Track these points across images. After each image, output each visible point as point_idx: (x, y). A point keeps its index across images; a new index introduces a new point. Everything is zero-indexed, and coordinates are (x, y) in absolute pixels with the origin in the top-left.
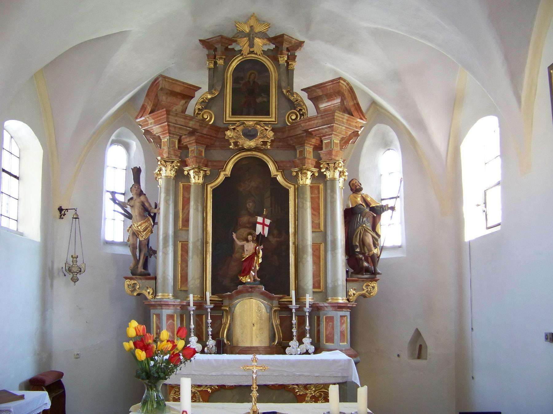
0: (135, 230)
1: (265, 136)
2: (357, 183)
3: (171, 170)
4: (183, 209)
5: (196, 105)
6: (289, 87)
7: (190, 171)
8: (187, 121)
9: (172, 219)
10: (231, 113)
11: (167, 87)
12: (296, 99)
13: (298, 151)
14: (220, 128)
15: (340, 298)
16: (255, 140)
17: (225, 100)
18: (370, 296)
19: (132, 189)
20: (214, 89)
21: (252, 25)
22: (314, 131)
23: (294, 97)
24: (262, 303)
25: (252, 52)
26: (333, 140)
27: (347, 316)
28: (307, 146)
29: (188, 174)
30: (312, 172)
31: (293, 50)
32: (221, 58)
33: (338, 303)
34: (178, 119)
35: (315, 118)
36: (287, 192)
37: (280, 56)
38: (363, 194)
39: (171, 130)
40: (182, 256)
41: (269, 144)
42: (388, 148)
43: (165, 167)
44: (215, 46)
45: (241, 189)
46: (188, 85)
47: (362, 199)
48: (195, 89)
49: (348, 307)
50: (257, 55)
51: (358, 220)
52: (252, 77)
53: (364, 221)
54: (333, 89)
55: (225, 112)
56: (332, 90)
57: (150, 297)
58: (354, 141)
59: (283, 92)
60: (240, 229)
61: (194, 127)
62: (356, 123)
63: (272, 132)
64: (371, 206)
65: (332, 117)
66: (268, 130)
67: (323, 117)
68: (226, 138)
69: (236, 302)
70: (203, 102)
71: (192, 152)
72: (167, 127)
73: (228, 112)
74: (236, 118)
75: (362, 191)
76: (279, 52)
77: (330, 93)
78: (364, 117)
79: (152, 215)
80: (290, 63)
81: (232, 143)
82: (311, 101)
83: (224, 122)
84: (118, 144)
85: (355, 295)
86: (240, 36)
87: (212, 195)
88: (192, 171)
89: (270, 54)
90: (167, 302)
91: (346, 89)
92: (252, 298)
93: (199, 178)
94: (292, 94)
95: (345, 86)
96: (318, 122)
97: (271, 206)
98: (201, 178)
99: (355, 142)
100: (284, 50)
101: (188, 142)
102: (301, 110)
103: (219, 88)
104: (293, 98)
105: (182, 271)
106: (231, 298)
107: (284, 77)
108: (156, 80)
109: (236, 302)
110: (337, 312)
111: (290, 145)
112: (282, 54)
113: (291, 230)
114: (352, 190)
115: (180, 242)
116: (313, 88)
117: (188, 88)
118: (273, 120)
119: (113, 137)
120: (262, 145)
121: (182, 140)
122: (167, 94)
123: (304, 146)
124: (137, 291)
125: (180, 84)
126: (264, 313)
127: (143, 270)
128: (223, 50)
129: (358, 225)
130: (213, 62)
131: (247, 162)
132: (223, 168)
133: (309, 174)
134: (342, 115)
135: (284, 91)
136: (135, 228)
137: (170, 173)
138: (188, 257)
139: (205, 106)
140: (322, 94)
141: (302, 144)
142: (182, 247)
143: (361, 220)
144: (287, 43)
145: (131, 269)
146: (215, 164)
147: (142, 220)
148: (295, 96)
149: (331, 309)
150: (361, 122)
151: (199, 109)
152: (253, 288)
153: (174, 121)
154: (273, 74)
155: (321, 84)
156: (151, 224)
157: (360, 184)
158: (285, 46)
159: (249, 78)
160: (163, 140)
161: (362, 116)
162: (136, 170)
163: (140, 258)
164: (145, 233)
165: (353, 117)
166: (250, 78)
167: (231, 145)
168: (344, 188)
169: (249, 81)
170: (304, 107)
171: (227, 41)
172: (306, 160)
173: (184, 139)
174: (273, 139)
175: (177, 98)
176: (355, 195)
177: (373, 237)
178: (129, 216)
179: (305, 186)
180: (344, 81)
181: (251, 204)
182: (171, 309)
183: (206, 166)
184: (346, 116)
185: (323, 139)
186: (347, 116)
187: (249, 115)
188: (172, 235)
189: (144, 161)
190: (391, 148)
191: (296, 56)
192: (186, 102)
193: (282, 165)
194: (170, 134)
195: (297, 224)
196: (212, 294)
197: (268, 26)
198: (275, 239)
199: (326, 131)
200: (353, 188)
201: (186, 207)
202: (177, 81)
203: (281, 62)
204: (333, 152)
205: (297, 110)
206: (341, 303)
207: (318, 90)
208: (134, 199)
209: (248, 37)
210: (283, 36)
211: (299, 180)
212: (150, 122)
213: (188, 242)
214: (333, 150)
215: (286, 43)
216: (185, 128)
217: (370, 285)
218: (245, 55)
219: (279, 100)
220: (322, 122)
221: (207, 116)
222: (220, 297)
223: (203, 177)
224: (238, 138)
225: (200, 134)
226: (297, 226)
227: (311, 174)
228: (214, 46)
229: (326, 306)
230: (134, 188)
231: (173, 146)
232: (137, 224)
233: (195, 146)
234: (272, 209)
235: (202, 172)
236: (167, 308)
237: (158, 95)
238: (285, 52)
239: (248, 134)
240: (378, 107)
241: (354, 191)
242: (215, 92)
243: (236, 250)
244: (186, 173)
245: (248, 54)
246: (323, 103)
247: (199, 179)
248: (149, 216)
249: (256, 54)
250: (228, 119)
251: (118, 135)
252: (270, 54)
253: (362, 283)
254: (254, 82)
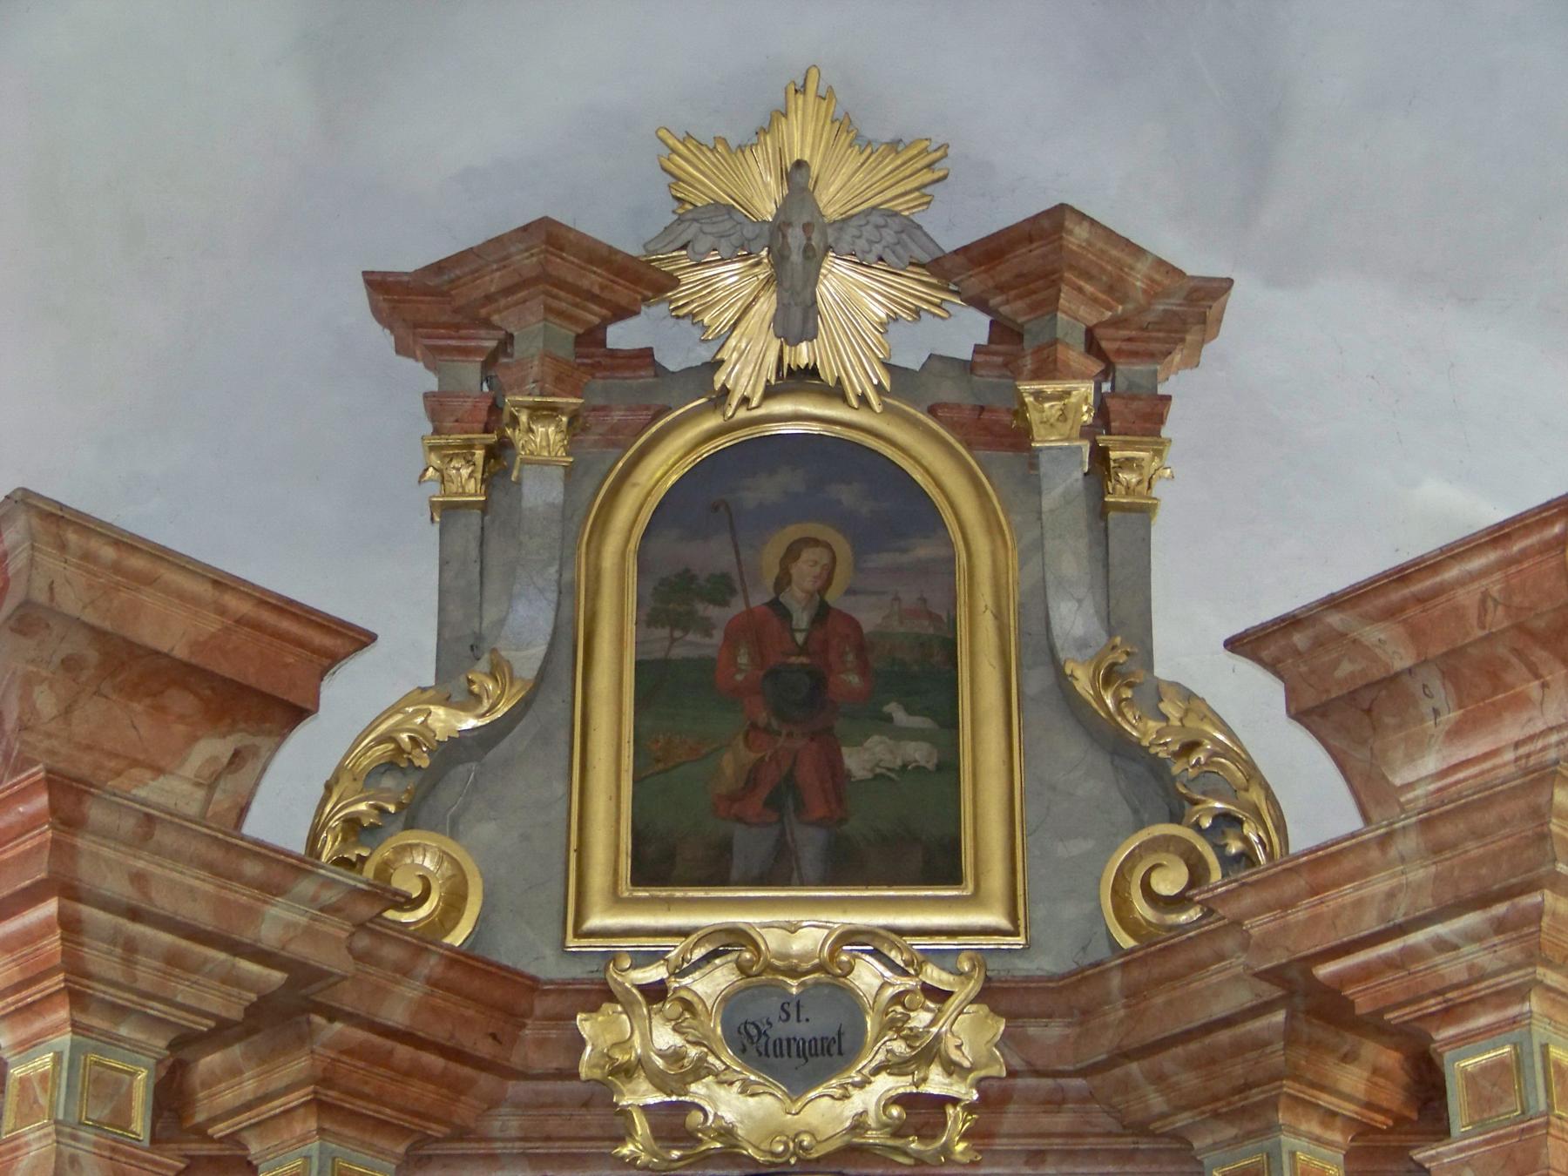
1: (929, 1047)
6: (1118, 640)
8: (241, 895)
11: (71, 601)
12: (1188, 738)
14: (533, 986)
16: (842, 1086)
20: (484, 665)
22: (1366, 973)
23: (1166, 718)
25: (800, 379)
26: (1545, 1048)
32: (543, 412)
34: (158, 871)
35: (1374, 854)
37: (1036, 386)
39: (93, 968)
41: (956, 1120)
46: (262, 603)
48: (327, 641)
50: (843, 398)
52: (806, 570)
54: (1508, 607)
55: (573, 856)
56: (1500, 611)
63: (983, 1009)
65: (1529, 829)
67: (1446, 831)
70: (389, 766)
72: (53, 943)
74: (670, 904)
76: (1028, 363)
77: (1488, 638)
80: (1113, 455)
81: (641, 1125)
82: (1308, 727)
94: (1153, 695)
96: (1400, 888)
100: (1067, 345)
101: (248, 1106)
102: (1227, 821)
104: (1153, 725)
111: (1141, 1129)
116: (1335, 619)
117: (257, 626)
120: (898, 1131)
128: (566, 351)
135: (1083, 683)
139: (404, 798)
140: (1408, 662)
144: (1088, 288)
148: (1171, 709)
151: (353, 826)
153: (116, 886)
154: (981, 545)
155: (1401, 575)
159: (783, 581)
160: (16, 1072)
166: (789, 583)
169: (777, 607)
170: (1256, 795)
171: (593, 280)
173: (209, 1083)
174: (999, 1070)
185: (1450, 1042)
187: (785, 882)
191: (1168, 398)
194: (84, 1009)
197: (929, 166)
199: (1471, 968)
202: (161, 555)
204: (1550, 1141)
205: (1197, 827)
207: (1373, 634)
210: (1059, 228)
214: (1548, 1124)
215: (1080, 290)
216: (222, 956)
220: (1437, 877)
224: (699, 1070)
225: (359, 1035)
231: (102, 1113)
233: (314, 1146)
238: (1074, 355)
239: (780, 1030)
245: (770, 393)
246: (1417, 748)
249: (836, 393)
252: (949, 391)
254: (823, 613)
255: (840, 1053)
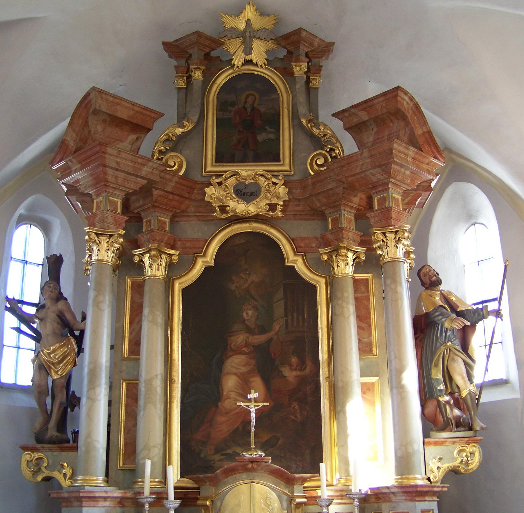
0: (44, 360)
2: (432, 272)
3: (108, 250)
4: (131, 323)
5: (156, 145)
6: (311, 114)
7: (143, 256)
9: (108, 336)
10: (214, 159)
11: (103, 109)
13: (330, 219)
15: (418, 476)
17: (205, 142)
18: (468, 470)
19: (45, 290)
20: (186, 119)
21: (249, 18)
24: (272, 489)
26: (392, 194)
27: (433, 510)
28: (345, 210)
29: (141, 260)
30: (355, 254)
31: (316, 58)
33: (416, 486)
34: (122, 161)
36: (312, 289)
38: (442, 290)
40: (127, 405)
41: (279, 208)
42: (473, 221)
43: (97, 244)
44: (188, 51)
45: (233, 287)
47: (443, 299)
48: (153, 115)
49: (434, 493)
50: (258, 66)
51: (439, 335)
53: (449, 336)
57: (66, 483)
58: (424, 201)
59: (301, 123)
60: (231, 356)
61: (149, 177)
62: (428, 164)
64: (458, 310)
66: (278, 184)
68: (207, 198)
69: (223, 489)
70: (167, 140)
71: (148, 224)
73: (209, 156)
74: (223, 166)
75: (441, 286)
76: (294, 59)
78: (441, 155)
79: (77, 333)
80: (311, 77)
83: (203, 174)
84: (32, 223)
85: (442, 470)
86: (229, 35)
87: (181, 298)
88: (148, 255)
89: (279, 65)
90: (91, 492)
91: (408, 108)
92: (255, 482)
93: (159, 267)
95: (407, 103)
97: (286, 315)
98: (162, 268)
99: (425, 203)
100: (301, 56)
102: (332, 150)
103: (195, 118)
104: (318, 131)
105: (128, 433)
106: (215, 482)
107: (302, 98)
108: (86, 96)
109: (223, 489)
110: (414, 502)
112: (298, 60)
113: (323, 355)
114: (423, 284)
115: (124, 380)
116: (353, 110)
117: (141, 113)
118: (287, 168)
119: (21, 210)
121: (132, 204)
122: (104, 121)
123: (340, 209)
124: (43, 472)
125: (127, 105)
126: (277, 510)
127: (55, 434)
128: (202, 57)
129: (438, 344)
130: (185, 78)
131: (243, 241)
132: (201, 252)
133: (351, 256)
134: (405, 147)
135: (304, 121)
136: (44, 357)
137: (105, 255)
138: (137, 408)
141: (336, 207)
142: (127, 390)
143: (444, 334)
145: (35, 431)
146: (188, 244)
147: (57, 343)
149: (404, 498)
150: (435, 163)
151: (160, 152)
152: (255, 461)
153: (114, 165)
156: (74, 350)
157: (437, 274)
158: (303, 49)
159: (246, 102)
161: (436, 154)
162: (53, 260)
163: (52, 412)
164: (61, 365)
165: (423, 154)
167: (215, 211)
168: (410, 280)
169: (244, 107)
171: (207, 43)
172: (344, 232)
175: (122, 129)
176: (429, 292)
177: (466, 363)
178: (37, 338)
179: (344, 278)
180: (406, 93)
181: (250, 312)
182: (99, 506)
183: (173, 248)
184: (412, 151)
186: (413, 151)
188: (106, 367)
189: (73, 250)
190: (479, 221)
192: (137, 139)
193: (302, 244)
195: (331, 344)
196: (182, 476)
198: (294, 373)
200: (426, 280)
201: (137, 320)
203: (297, 74)
205: (326, 151)
206: (422, 486)
208: (47, 307)
209: (242, 37)
210: (300, 32)
211: (333, 268)
212: (73, 169)
213: (138, 380)
217: (467, 449)
218: (238, 67)
219: (294, 137)
221: (174, 161)
222: (196, 481)
223: (166, 265)
226: (333, 348)
227: (354, 257)
228: (187, 52)
229: (393, 493)
230: (48, 288)
232: (48, 350)
234: (287, 321)
235: (163, 256)
236: (92, 503)
237: (90, 123)
238: (303, 58)
239: (244, 191)
240: (454, 156)
241: (428, 286)
242: (187, 123)
243: (225, 393)
244: (137, 259)
247: (158, 270)
248: (71, 336)
249: (256, 65)
250: (209, 169)
251: (31, 208)
252: (279, 65)
253: (451, 447)
254: (253, 109)
255: (256, 195)
